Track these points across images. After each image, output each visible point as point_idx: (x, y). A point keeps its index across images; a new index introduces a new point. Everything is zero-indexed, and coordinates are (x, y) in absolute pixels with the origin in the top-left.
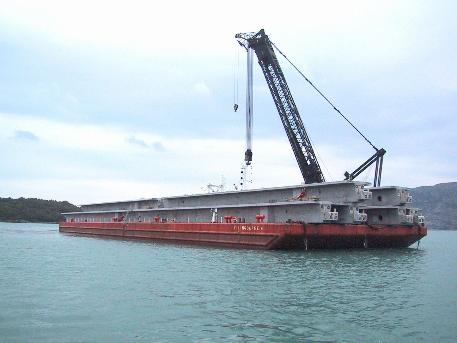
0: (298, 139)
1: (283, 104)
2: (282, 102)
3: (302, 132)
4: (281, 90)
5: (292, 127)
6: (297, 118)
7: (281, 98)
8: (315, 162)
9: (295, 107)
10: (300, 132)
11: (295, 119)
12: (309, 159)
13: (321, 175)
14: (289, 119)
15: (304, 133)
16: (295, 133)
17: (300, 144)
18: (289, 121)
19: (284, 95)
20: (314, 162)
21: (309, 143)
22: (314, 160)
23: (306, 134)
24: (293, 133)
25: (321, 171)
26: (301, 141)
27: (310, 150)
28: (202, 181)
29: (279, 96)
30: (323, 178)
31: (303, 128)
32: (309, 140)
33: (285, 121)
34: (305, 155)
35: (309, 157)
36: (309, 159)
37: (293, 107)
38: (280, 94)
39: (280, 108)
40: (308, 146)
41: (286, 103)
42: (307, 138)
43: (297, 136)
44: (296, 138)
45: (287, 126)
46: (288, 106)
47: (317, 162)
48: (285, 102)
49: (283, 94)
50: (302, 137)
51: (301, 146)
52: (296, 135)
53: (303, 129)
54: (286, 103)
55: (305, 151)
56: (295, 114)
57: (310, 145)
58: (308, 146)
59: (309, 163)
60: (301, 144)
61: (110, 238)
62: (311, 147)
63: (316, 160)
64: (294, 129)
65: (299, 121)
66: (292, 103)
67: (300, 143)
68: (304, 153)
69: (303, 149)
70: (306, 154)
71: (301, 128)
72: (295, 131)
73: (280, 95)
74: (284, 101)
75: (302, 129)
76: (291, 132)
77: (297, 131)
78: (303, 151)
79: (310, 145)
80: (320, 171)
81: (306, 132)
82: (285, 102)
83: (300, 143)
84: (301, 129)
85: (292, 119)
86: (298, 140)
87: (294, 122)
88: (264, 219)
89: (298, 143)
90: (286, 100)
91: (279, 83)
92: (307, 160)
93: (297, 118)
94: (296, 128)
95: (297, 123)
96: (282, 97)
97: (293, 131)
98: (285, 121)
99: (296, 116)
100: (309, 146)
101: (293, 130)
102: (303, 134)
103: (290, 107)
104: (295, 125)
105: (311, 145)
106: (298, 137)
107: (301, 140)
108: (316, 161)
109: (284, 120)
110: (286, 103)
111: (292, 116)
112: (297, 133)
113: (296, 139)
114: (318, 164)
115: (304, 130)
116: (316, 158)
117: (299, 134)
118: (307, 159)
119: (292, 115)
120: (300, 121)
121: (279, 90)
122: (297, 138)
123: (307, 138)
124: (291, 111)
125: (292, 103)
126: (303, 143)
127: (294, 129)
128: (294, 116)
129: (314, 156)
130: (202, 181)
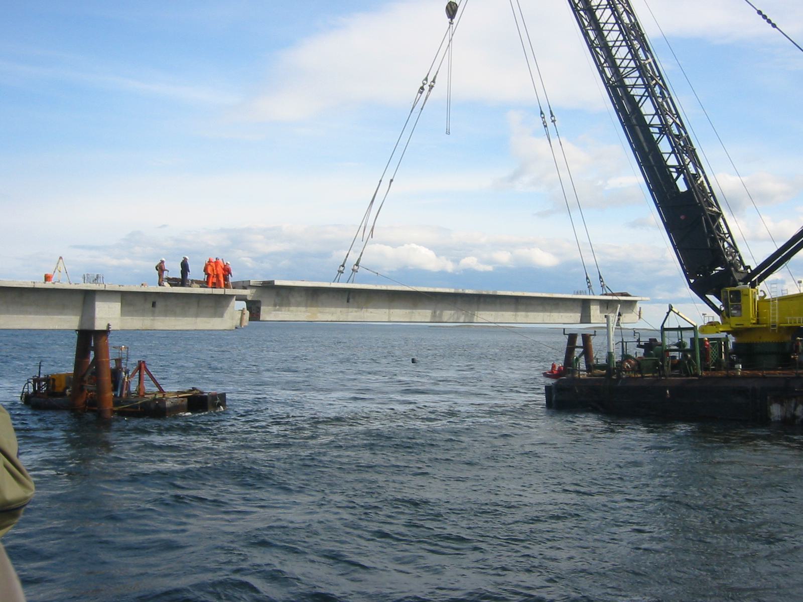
0: (646, 117)
1: (614, 51)
2: (611, 44)
3: (658, 95)
4: (605, 9)
5: (628, 82)
6: (641, 52)
7: (605, 33)
8: (702, 181)
9: (633, 21)
10: (652, 95)
11: (635, 57)
12: (682, 176)
13: (721, 220)
14: (616, 57)
15: (664, 97)
16: (637, 99)
17: (652, 129)
18: (618, 62)
19: (631, 58)
20: (699, 182)
21: (681, 126)
22: (695, 177)
23: (671, 99)
24: (631, 99)
25: (720, 210)
26: (656, 121)
27: (685, 147)
28: (413, 361)
29: (602, 25)
30: (726, 231)
31: (660, 82)
32: (679, 117)
33: (605, 65)
34: (669, 163)
35: (681, 169)
36: (682, 176)
37: (676, 132)
38: (603, 20)
39: (590, 25)
40: (677, 136)
41: (620, 46)
42: (674, 112)
43: (642, 109)
44: (640, 112)
45: (613, 79)
46: (629, 56)
47: (708, 184)
48: (618, 44)
49: (612, 20)
50: (660, 111)
51: (656, 136)
52: (640, 105)
53: (660, 86)
54: (620, 46)
55: (670, 150)
56: (635, 42)
57: (683, 132)
58: (679, 137)
59: (682, 186)
60: (657, 130)
61: (140, 543)
62: (688, 140)
63: (705, 177)
64: (633, 86)
65: (646, 62)
66: (674, 122)
67: (652, 126)
68: (665, 156)
69: (664, 146)
70: (672, 161)
71: (654, 82)
72: (637, 92)
73: (605, 24)
74: (617, 40)
75: (657, 86)
76: (624, 98)
77: (641, 91)
78: (662, 150)
79: (683, 132)
80: (717, 210)
81: (669, 94)
82: (618, 44)
83: (652, 126)
84: (655, 85)
85: (625, 59)
86: (648, 119)
87: (632, 64)
88: (560, 364)
89: (645, 127)
90: (621, 38)
91: (614, 22)
92: (677, 178)
93: (641, 52)
94: (640, 81)
95: (641, 68)
96: (617, 42)
97: (632, 93)
98: (605, 65)
99: (639, 46)
100: (682, 134)
101: (629, 89)
102: (660, 100)
103: (618, 19)
104: (637, 74)
105: (686, 133)
106: (647, 108)
107: (656, 117)
108: (702, 178)
109: (602, 61)
110: (606, 10)
111: (626, 48)
112: (644, 98)
113: (641, 117)
114: (710, 188)
115: (663, 87)
116: (703, 172)
117: (665, 136)
118: (675, 175)
119: (627, 43)
120: (650, 60)
121: (600, 7)
122: (644, 113)
123: (674, 112)
124: (621, 32)
125: (674, 122)
126: (664, 129)
127: (633, 86)
128: (631, 47)
129: (697, 164)
130: (413, 361)
